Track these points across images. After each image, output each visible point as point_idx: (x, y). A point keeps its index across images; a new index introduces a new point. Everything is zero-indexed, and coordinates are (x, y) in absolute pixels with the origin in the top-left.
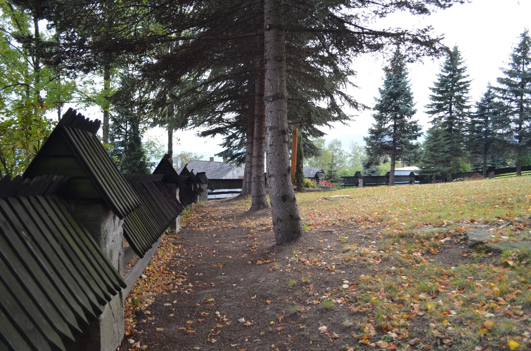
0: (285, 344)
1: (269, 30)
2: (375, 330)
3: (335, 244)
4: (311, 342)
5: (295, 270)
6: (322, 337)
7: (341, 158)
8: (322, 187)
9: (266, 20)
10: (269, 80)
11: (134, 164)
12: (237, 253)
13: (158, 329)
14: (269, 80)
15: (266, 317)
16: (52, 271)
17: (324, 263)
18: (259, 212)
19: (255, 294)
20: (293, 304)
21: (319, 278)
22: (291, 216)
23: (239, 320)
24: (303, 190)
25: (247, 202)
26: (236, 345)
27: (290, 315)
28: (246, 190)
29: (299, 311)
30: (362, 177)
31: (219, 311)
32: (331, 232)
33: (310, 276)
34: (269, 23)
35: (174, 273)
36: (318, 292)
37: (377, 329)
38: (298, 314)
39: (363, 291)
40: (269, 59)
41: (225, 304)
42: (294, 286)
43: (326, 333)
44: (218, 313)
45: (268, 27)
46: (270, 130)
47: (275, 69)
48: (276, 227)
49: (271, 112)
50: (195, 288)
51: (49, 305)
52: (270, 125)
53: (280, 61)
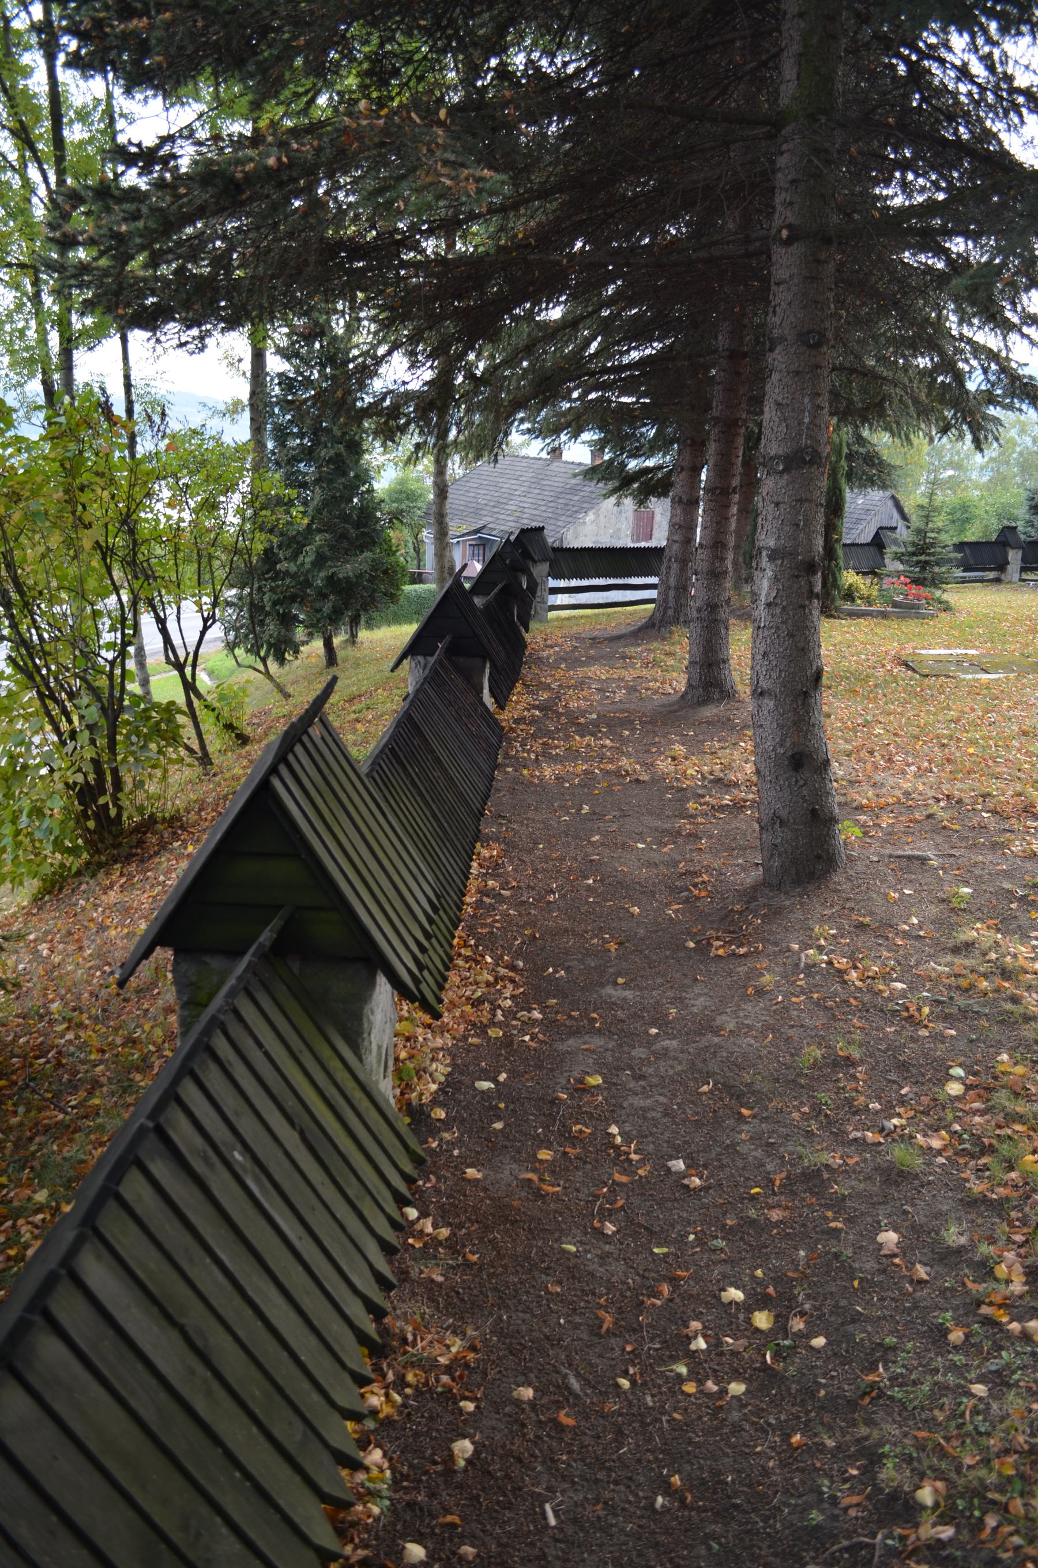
0: (790, 1274)
1: (788, 242)
2: (1026, 1274)
3: (933, 910)
4: (856, 1283)
5: (817, 1004)
6: (884, 1271)
7: (958, 453)
8: (895, 604)
9: (779, 208)
10: (778, 404)
11: (345, 518)
12: (653, 894)
13: (471, 1172)
14: (778, 404)
15: (740, 1163)
16: (301, 1230)
17: (899, 986)
18: (709, 712)
19: (709, 1075)
20: (809, 1134)
21: (883, 1047)
22: (814, 812)
23: (670, 1164)
24: (837, 609)
25: (669, 654)
26: (665, 1250)
27: (803, 1174)
28: (666, 609)
29: (827, 1166)
30: (1018, 546)
31: (616, 1123)
32: (923, 860)
33: (858, 1036)
34: (791, 219)
35: (489, 959)
36: (879, 1099)
37: (1031, 1273)
38: (826, 1176)
39: (1000, 1118)
40: (782, 339)
41: (631, 1100)
42: (814, 1066)
43: (897, 1261)
44: (614, 1129)
45: (785, 233)
46: (772, 558)
47: (797, 373)
48: (767, 837)
49: (777, 504)
50: (549, 1025)
51: (313, 1341)
52: (772, 543)
53: (817, 345)
